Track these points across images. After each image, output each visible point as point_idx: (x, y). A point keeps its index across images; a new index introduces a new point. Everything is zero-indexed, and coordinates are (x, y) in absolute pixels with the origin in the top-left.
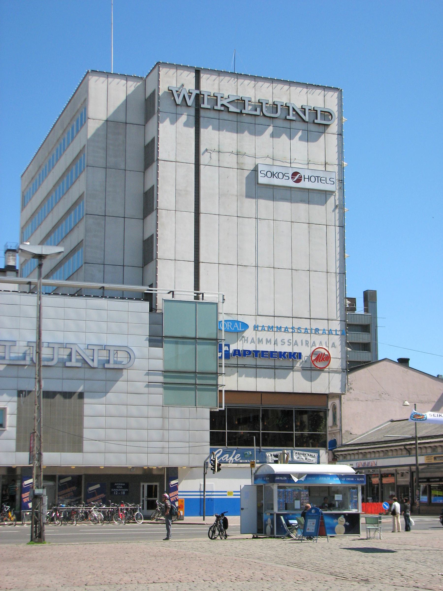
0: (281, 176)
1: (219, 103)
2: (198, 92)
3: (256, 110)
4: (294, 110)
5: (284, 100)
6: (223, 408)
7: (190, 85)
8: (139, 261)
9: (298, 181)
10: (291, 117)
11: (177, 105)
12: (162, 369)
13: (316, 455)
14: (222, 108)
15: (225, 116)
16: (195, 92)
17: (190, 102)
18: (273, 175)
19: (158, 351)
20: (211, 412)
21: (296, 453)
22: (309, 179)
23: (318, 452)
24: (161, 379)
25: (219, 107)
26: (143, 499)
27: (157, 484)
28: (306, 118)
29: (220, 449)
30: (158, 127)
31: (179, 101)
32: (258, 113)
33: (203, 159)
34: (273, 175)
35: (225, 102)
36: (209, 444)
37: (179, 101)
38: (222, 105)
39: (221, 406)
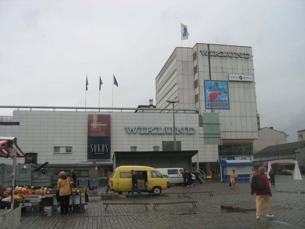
0: (236, 78)
1: (215, 54)
2: (209, 51)
3: (226, 55)
4: (238, 54)
5: (234, 51)
6: (222, 144)
7: (207, 49)
8: (194, 102)
9: (241, 79)
10: (237, 56)
11: (203, 55)
12: (203, 133)
13: (250, 157)
14: (216, 55)
15: (217, 57)
16: (208, 51)
17: (207, 54)
18: (234, 77)
19: (202, 128)
20: (218, 145)
21: (69, 150)
22: (245, 78)
23: (250, 157)
24: (203, 136)
25: (215, 55)
26: (151, 204)
27: (203, 167)
28: (242, 56)
29: (221, 157)
30: (210, 109)
31: (203, 54)
32: (227, 56)
33: (212, 70)
34: (234, 77)
35: (217, 53)
36: (182, 143)
37: (203, 54)
38: (216, 54)
39: (221, 143)
